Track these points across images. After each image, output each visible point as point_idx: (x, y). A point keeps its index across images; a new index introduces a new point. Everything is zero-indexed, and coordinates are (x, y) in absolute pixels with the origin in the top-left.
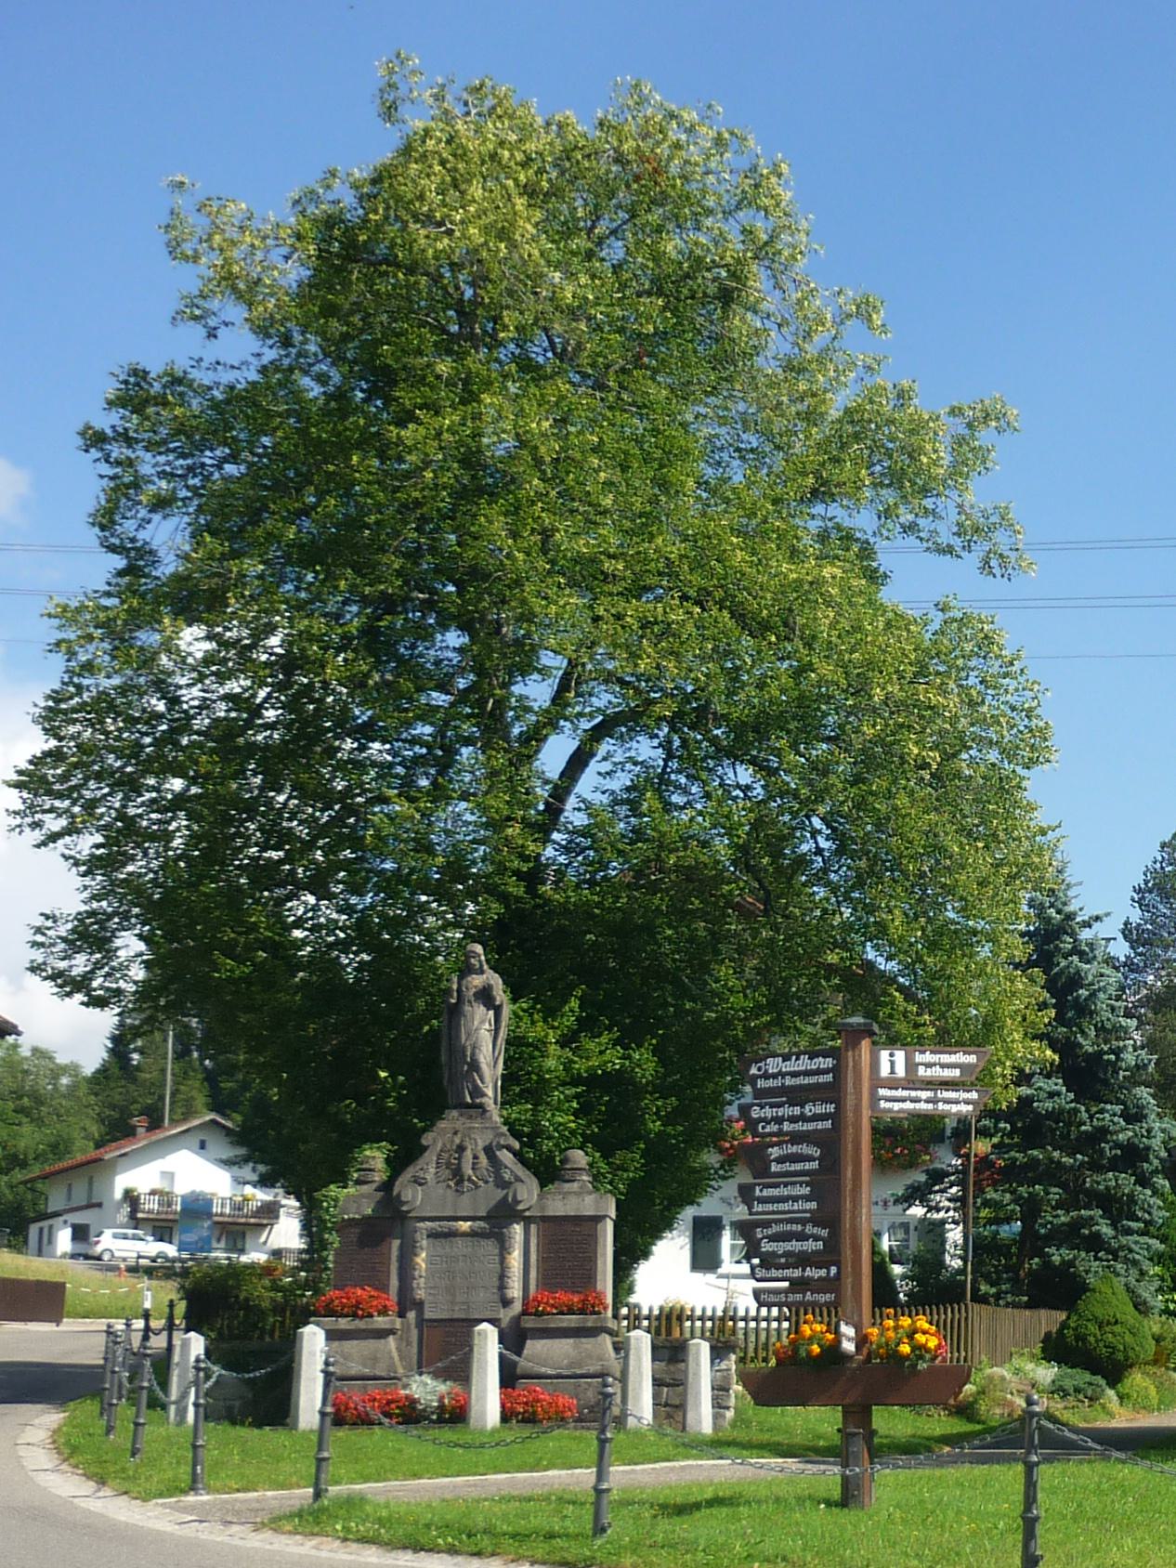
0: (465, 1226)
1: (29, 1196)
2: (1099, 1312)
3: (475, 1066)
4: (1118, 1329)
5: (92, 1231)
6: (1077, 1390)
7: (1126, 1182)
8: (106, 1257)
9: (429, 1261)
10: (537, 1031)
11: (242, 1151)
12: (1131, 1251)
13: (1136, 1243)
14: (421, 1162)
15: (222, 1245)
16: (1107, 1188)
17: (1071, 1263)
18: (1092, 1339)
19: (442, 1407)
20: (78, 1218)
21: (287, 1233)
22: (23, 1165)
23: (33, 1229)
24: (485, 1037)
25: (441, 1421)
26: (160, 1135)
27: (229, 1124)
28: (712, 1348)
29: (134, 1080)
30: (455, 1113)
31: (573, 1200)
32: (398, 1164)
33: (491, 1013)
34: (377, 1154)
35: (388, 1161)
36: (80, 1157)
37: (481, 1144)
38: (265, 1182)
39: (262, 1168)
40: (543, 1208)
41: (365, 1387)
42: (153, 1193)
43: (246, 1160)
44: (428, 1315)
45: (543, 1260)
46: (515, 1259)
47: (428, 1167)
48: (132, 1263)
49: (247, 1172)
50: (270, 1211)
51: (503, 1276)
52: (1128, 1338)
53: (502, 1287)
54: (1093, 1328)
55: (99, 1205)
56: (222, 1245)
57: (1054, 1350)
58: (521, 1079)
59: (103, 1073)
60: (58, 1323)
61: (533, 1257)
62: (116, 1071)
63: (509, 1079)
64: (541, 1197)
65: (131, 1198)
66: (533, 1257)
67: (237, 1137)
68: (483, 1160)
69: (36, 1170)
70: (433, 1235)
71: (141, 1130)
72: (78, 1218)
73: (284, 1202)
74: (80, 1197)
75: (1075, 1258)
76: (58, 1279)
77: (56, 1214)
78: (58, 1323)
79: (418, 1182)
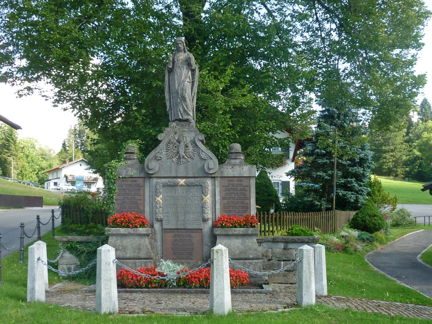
0: (182, 182)
1: (45, 176)
2: (369, 212)
3: (184, 99)
4: (376, 218)
5: (58, 184)
6: (368, 239)
7: (361, 170)
8: (61, 189)
9: (163, 199)
10: (212, 85)
11: (89, 166)
12: (363, 191)
13: (364, 189)
14: (158, 149)
15: (86, 187)
16: (356, 171)
17: (344, 195)
18: (367, 221)
19: (179, 279)
20: (55, 181)
21: (100, 184)
22: (44, 169)
23: (46, 183)
24: (188, 85)
25: (179, 286)
26: (71, 163)
27: (86, 160)
28: (327, 249)
29: (67, 153)
30: (174, 124)
31: (237, 168)
32: (146, 150)
33: (190, 73)
34: (135, 145)
35: (140, 149)
36: (55, 168)
37: (188, 140)
38: (95, 173)
39: (94, 170)
40: (222, 172)
41: (135, 263)
42: (71, 175)
43: (90, 168)
44: (165, 227)
45: (223, 198)
46: (208, 198)
47: (161, 150)
48: (66, 191)
49: (90, 171)
50: (96, 179)
51: (203, 207)
52: (380, 221)
53: (203, 212)
54: (368, 218)
55: (59, 178)
56: (86, 187)
57: (354, 224)
58: (203, 112)
59: (61, 152)
60: (41, 206)
61: (218, 198)
62: (63, 151)
63: (198, 110)
64: (220, 168)
65: (66, 177)
66: (218, 198)
67: (88, 163)
68: (191, 148)
69: (46, 170)
70: (165, 186)
71: (67, 162)
72: (55, 181)
73: (99, 177)
74: (55, 177)
75: (347, 193)
76: (40, 196)
77: (50, 180)
78: (42, 206)
79: (156, 158)
